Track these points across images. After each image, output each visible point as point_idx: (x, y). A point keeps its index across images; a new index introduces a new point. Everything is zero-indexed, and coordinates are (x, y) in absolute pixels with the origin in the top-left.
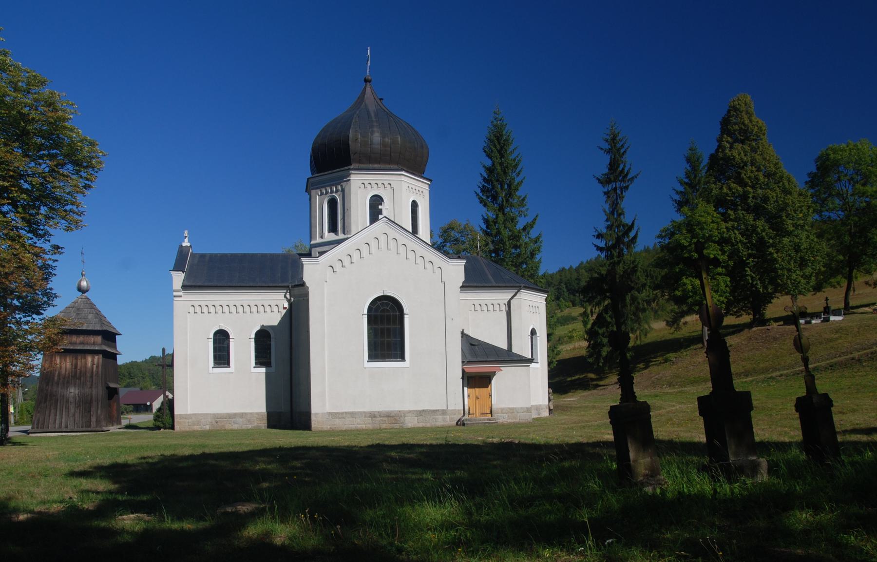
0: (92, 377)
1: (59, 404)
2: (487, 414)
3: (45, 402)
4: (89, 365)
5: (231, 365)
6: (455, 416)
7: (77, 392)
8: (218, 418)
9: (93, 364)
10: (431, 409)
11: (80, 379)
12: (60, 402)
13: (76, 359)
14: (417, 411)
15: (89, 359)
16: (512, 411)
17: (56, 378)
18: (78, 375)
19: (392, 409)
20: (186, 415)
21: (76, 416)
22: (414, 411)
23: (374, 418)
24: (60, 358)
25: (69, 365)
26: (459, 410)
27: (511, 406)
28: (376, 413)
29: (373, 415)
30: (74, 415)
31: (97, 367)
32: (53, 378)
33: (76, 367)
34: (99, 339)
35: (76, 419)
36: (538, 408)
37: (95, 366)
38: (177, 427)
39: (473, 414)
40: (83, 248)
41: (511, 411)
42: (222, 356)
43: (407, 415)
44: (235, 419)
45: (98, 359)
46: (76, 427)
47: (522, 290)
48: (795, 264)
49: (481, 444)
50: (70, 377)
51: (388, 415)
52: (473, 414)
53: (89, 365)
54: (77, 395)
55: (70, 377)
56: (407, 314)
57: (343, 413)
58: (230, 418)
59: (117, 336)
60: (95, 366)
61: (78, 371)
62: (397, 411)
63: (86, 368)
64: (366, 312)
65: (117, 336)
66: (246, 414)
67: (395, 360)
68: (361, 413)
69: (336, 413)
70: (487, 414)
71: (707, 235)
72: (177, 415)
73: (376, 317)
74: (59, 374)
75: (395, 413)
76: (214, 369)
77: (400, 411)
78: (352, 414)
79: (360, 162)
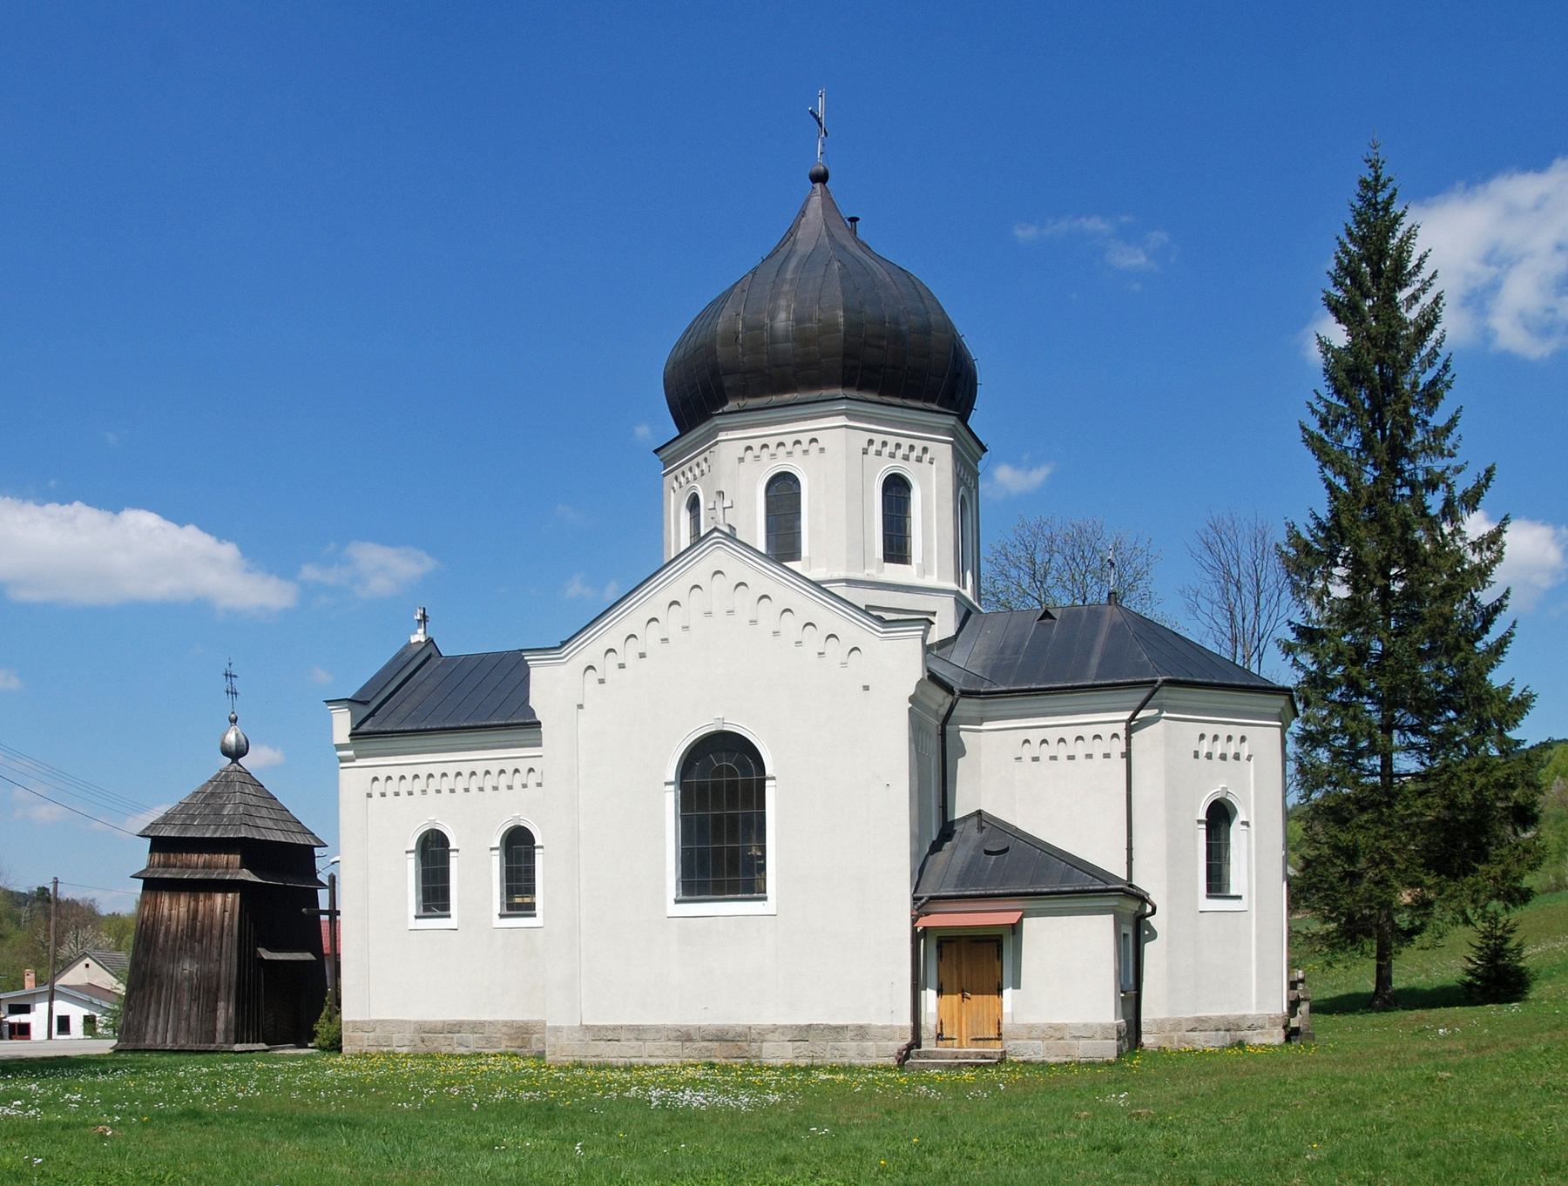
0: (221, 937)
1: (164, 992)
2: (988, 1039)
3: (142, 987)
5: (768, 894)
6: (890, 1043)
8: (426, 1030)
9: (225, 911)
10: (831, 1023)
11: (200, 941)
12: (167, 990)
14: (791, 1027)
15: (219, 898)
16: (1055, 1032)
17: (161, 940)
19: (732, 1022)
20: (364, 1022)
21: (192, 1020)
22: (786, 1027)
23: (688, 1044)
24: (170, 899)
25: (183, 910)
26: (901, 1028)
27: (1058, 1020)
28: (692, 1032)
29: (685, 1036)
30: (188, 1018)
31: (232, 916)
32: (157, 941)
33: (195, 918)
34: (236, 859)
36: (1086, 1033)
38: (346, 1048)
39: (952, 1039)
40: (230, 664)
41: (1058, 1035)
42: (435, 896)
43: (768, 1037)
44: (459, 1035)
47: (722, 436)
50: (184, 938)
51: (721, 1036)
52: (952, 1039)
54: (195, 976)
55: (184, 938)
56: (773, 778)
57: (615, 1028)
58: (449, 1032)
60: (227, 914)
61: (198, 924)
62: (743, 1026)
64: (671, 775)
66: (482, 1024)
67: (747, 896)
68: (657, 1029)
69: (600, 1028)
70: (988, 1039)
71: (1512, 781)
72: (347, 1022)
73: (702, 789)
74: (168, 929)
75: (739, 1030)
76: (418, 920)
77: (750, 1028)
78: (638, 1032)
79: (744, 392)
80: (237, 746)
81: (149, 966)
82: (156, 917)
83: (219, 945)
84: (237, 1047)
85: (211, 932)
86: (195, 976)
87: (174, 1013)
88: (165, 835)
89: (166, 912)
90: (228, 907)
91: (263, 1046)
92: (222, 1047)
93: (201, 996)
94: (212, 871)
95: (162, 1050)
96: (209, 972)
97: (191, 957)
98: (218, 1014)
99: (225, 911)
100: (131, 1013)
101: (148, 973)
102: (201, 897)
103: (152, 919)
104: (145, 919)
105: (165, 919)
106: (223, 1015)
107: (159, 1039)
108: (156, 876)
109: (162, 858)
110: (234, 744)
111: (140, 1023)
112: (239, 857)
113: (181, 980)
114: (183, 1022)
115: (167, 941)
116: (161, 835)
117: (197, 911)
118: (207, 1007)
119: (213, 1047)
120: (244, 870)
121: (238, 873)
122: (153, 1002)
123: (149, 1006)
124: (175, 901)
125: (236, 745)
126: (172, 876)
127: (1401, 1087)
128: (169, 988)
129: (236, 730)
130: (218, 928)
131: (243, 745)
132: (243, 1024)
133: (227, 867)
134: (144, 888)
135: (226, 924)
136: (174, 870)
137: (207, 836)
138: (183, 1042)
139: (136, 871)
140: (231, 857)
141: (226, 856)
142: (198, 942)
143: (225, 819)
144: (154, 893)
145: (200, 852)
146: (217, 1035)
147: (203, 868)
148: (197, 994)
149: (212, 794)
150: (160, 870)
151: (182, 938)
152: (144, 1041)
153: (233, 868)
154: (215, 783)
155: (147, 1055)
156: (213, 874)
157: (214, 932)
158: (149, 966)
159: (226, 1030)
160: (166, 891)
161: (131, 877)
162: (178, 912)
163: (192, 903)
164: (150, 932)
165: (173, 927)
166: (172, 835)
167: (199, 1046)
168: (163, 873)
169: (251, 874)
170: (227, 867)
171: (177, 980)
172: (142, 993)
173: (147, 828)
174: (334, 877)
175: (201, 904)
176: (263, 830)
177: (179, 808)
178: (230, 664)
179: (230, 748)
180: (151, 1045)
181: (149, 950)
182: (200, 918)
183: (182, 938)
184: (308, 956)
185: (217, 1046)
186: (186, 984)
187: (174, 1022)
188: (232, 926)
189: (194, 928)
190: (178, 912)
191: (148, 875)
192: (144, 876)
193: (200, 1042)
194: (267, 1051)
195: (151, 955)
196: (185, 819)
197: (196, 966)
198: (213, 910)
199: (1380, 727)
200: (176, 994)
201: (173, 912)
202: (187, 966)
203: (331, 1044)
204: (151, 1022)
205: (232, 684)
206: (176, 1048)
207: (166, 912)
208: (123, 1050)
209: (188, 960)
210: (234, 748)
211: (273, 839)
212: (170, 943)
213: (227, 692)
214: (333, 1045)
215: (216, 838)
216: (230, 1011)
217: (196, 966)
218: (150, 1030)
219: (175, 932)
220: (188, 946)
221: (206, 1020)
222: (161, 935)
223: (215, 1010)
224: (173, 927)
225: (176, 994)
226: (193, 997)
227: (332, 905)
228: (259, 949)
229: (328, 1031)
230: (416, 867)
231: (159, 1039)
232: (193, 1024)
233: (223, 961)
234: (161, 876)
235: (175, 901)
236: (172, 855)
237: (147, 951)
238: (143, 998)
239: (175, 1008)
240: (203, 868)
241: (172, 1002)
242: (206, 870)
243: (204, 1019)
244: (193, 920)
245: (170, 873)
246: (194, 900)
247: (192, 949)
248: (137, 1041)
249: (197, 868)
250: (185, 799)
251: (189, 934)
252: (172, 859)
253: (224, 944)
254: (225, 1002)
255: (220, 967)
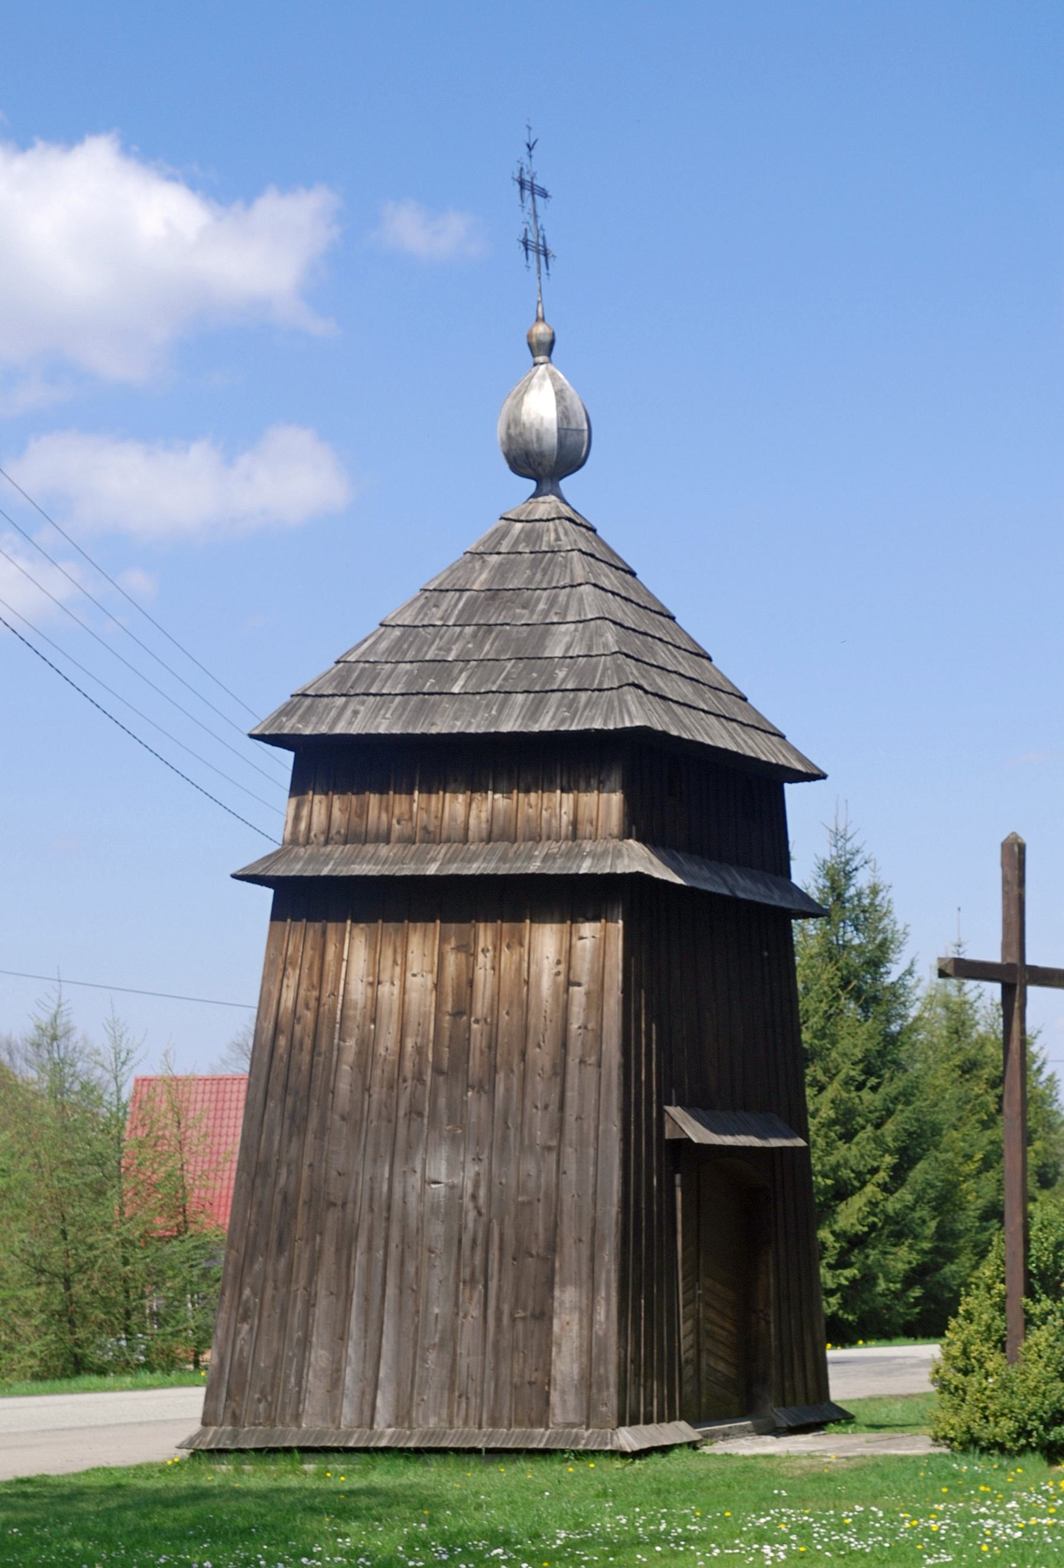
0: (560, 1070)
1: (359, 1258)
4: (546, 983)
7: (466, 1179)
9: (570, 983)
11: (486, 1086)
12: (370, 1248)
13: (467, 949)
17: (344, 1085)
18: (476, 1063)
21: (462, 1350)
24: (374, 947)
25: (420, 984)
30: (450, 1338)
31: (596, 998)
33: (463, 1010)
35: (463, 1363)
37: (578, 994)
40: (530, 148)
45: (604, 942)
46: (458, 1422)
48: (904, 1486)
49: (817, 901)
53: (546, 983)
54: (467, 1200)
55: (428, 1077)
59: (791, 790)
60: (578, 994)
63: (526, 1007)
65: (791, 790)
80: (563, 432)
81: (305, 1172)
82: (325, 1009)
83: (555, 1097)
84: (628, 1438)
85: (523, 1054)
86: (467, 1200)
87: (399, 1332)
88: (354, 730)
89: (358, 991)
90: (583, 968)
91: (679, 1431)
92: (577, 1439)
93: (494, 1267)
94: (523, 847)
95: (366, 1450)
96: (521, 1188)
97: (454, 1140)
98: (556, 1328)
99: (570, 983)
100: (246, 1327)
101: (304, 1195)
102: (485, 934)
103: (309, 1015)
104: (285, 1020)
105: (356, 1014)
106: (575, 1327)
107: (348, 1413)
108: (325, 871)
109: (336, 813)
110: (553, 426)
111: (277, 1362)
112: (617, 799)
113: (421, 1217)
114: (432, 1356)
115: (367, 1089)
116: (338, 730)
117: (471, 983)
118: (517, 1303)
119: (540, 1437)
120: (631, 841)
121: (618, 854)
122: (322, 1293)
123: (310, 1304)
124: (389, 953)
125: (559, 429)
126: (386, 870)
127: (857, 1485)
128: (379, 1242)
129: (553, 377)
130: (550, 1045)
131: (580, 431)
132: (636, 1361)
133: (574, 836)
134: (277, 914)
135: (574, 1026)
136: (384, 850)
137: (506, 728)
138: (433, 1421)
139: (248, 857)
140: (589, 800)
141: (568, 799)
142: (480, 1088)
143: (561, 674)
144: (318, 926)
145: (475, 785)
146: (555, 1397)
147: (489, 839)
148: (478, 1260)
149: (493, 593)
150: (338, 851)
151: (419, 1078)
152: (297, 1417)
153: (594, 837)
154: (494, 559)
155: (826, 1471)
156: (530, 858)
157: (533, 1051)
158: (305, 1172)
159: (588, 1383)
160: (356, 920)
161: (234, 876)
162: (404, 990)
163: (452, 960)
164: (306, 1057)
165: (388, 1040)
166: (382, 730)
167: (490, 1437)
168: (349, 861)
169: (656, 860)
170: (574, 835)
171: (405, 1216)
172: (283, 1262)
173: (287, 711)
174: (1022, 848)
175: (484, 961)
176: (674, 706)
177: (384, 645)
178: (530, 148)
179: (539, 439)
180: (321, 1434)
181: (306, 1119)
182: (481, 1007)
183: (419, 1078)
184: (800, 1142)
185: (557, 1437)
186: (437, 1230)
187: (398, 1354)
188: (599, 1037)
189: (461, 1046)
190: (404, 990)
191: (296, 869)
192: (280, 870)
193: (494, 1422)
194: (693, 1445)
195: (310, 1137)
196: (412, 679)
197: (472, 1169)
198: (526, 982)
199: (840, 987)
200: (402, 1264)
201: (385, 989)
202: (439, 1169)
203: (1023, 1432)
204: (319, 1356)
205: (536, 216)
206: (412, 1444)
207: (358, 991)
208: (594, 1453)
209: (444, 1151)
210: (551, 440)
211: (708, 742)
212: (378, 1093)
213: (525, 243)
214: (1029, 1434)
215: (542, 734)
216: (601, 1315)
217: (472, 1169)
218: (315, 1384)
219: (393, 1058)
220: (442, 1101)
221: (514, 1348)
222: (345, 1068)
223: (543, 1315)
224: (388, 1040)
225: (402, 1264)
226: (466, 1273)
227: (1015, 949)
228: (667, 1108)
229: (1004, 1386)
230: (1003, 865)
231: (348, 1413)
232: (468, 1360)
233: (569, 1152)
234: (344, 871)
235: (389, 953)
236: (374, 799)
237: (297, 1123)
238: (289, 1280)
239: (400, 1309)
240: (489, 839)
241: (391, 1291)
242: (502, 846)
243: (505, 1343)
244: (457, 1014)
245: (375, 859)
246: (458, 949)
247: (457, 1114)
248: (271, 1421)
249: (465, 840)
250: (400, 613)
251: (445, 1064)
252: (373, 813)
253: (571, 1095)
254: (578, 1284)
255: (560, 1171)
